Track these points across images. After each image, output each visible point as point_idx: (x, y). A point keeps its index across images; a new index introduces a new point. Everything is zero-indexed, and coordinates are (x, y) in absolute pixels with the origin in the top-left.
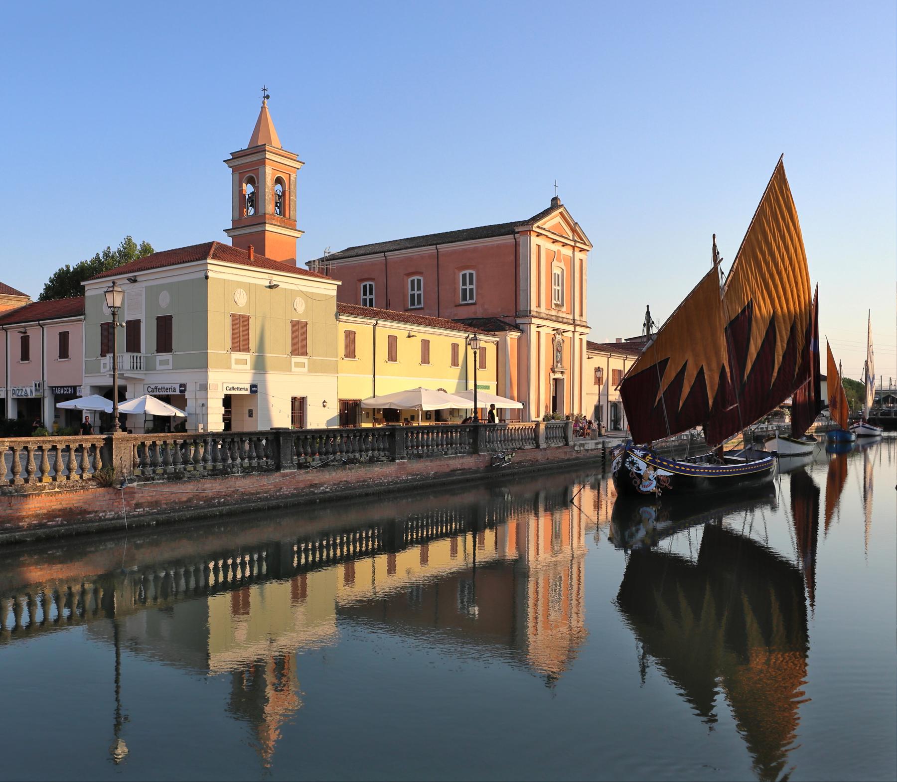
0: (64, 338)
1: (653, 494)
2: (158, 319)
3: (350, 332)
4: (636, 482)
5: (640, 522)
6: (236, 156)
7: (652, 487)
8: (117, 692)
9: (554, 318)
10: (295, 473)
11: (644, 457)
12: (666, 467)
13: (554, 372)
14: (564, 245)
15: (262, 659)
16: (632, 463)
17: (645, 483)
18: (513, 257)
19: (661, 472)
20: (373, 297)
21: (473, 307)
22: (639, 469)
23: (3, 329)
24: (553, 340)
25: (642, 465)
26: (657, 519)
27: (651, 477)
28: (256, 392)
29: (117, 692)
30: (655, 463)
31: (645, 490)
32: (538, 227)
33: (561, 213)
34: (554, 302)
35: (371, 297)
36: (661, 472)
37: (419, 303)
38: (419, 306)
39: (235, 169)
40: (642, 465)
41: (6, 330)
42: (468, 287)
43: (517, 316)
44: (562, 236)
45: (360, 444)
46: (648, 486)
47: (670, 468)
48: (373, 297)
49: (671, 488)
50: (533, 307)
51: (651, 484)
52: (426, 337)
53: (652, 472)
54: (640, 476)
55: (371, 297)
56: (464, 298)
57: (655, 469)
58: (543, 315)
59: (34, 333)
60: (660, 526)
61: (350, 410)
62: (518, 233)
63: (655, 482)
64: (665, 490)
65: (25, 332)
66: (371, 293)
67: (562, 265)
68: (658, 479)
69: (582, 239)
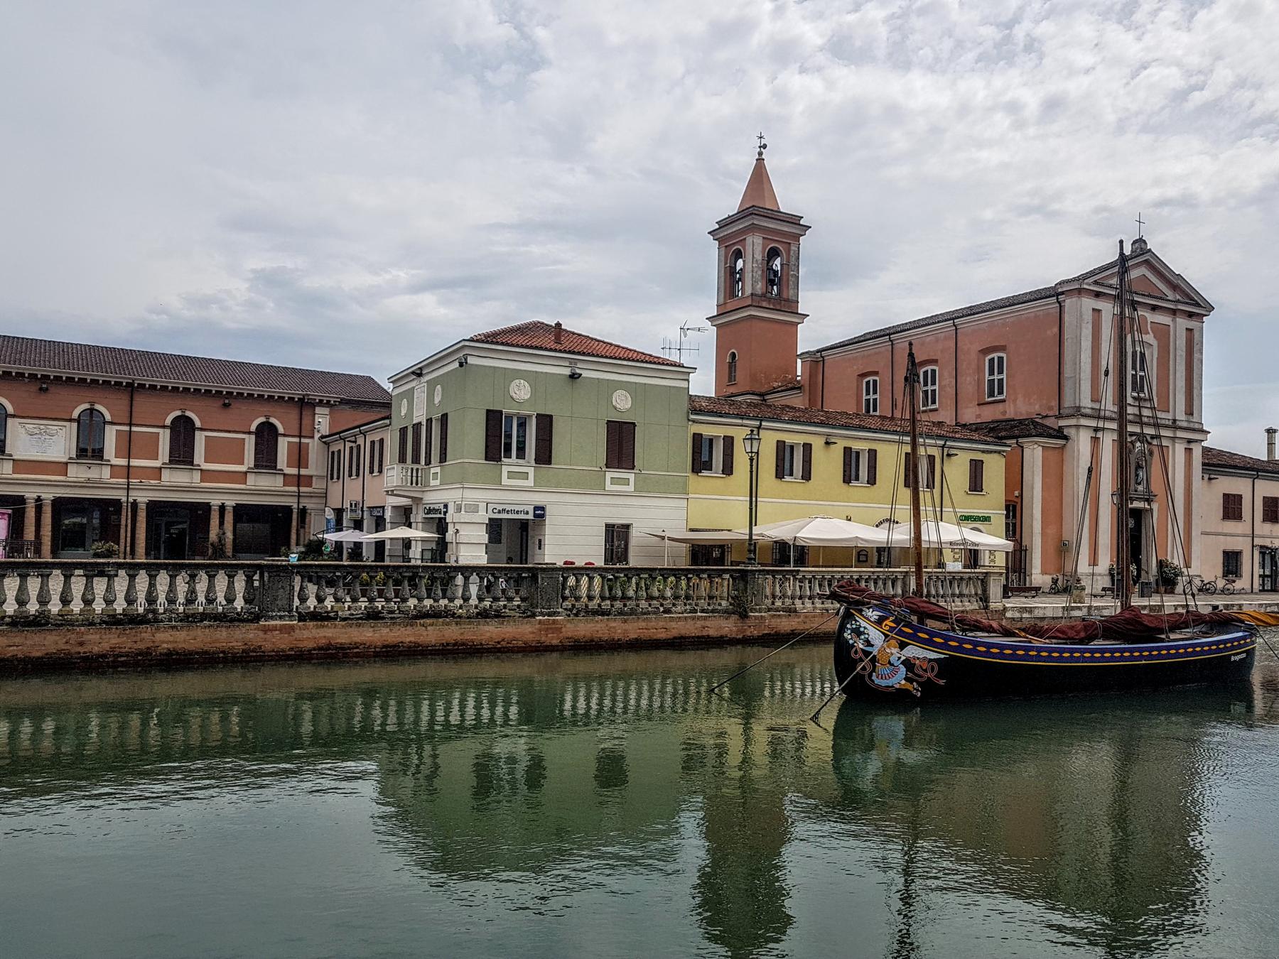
1: (902, 693)
2: (1225, 495)
5: (870, 746)
6: (723, 224)
7: (898, 680)
10: (292, 628)
11: (879, 622)
12: (929, 643)
15: (882, 842)
16: (858, 632)
17: (885, 670)
18: (1056, 330)
19: (913, 651)
20: (877, 396)
21: (1001, 405)
22: (868, 643)
25: (875, 635)
26: (908, 743)
27: (893, 659)
28: (543, 516)
30: (901, 633)
31: (883, 683)
32: (1096, 283)
36: (913, 651)
38: (933, 407)
39: (721, 241)
40: (875, 635)
42: (996, 377)
43: (1060, 417)
44: (1150, 296)
49: (942, 682)
51: (895, 672)
52: (979, 456)
53: (895, 651)
56: (991, 394)
57: (902, 646)
62: (1062, 293)
63: (903, 669)
64: (927, 686)
66: (875, 392)
68: (908, 664)
69: (1192, 299)
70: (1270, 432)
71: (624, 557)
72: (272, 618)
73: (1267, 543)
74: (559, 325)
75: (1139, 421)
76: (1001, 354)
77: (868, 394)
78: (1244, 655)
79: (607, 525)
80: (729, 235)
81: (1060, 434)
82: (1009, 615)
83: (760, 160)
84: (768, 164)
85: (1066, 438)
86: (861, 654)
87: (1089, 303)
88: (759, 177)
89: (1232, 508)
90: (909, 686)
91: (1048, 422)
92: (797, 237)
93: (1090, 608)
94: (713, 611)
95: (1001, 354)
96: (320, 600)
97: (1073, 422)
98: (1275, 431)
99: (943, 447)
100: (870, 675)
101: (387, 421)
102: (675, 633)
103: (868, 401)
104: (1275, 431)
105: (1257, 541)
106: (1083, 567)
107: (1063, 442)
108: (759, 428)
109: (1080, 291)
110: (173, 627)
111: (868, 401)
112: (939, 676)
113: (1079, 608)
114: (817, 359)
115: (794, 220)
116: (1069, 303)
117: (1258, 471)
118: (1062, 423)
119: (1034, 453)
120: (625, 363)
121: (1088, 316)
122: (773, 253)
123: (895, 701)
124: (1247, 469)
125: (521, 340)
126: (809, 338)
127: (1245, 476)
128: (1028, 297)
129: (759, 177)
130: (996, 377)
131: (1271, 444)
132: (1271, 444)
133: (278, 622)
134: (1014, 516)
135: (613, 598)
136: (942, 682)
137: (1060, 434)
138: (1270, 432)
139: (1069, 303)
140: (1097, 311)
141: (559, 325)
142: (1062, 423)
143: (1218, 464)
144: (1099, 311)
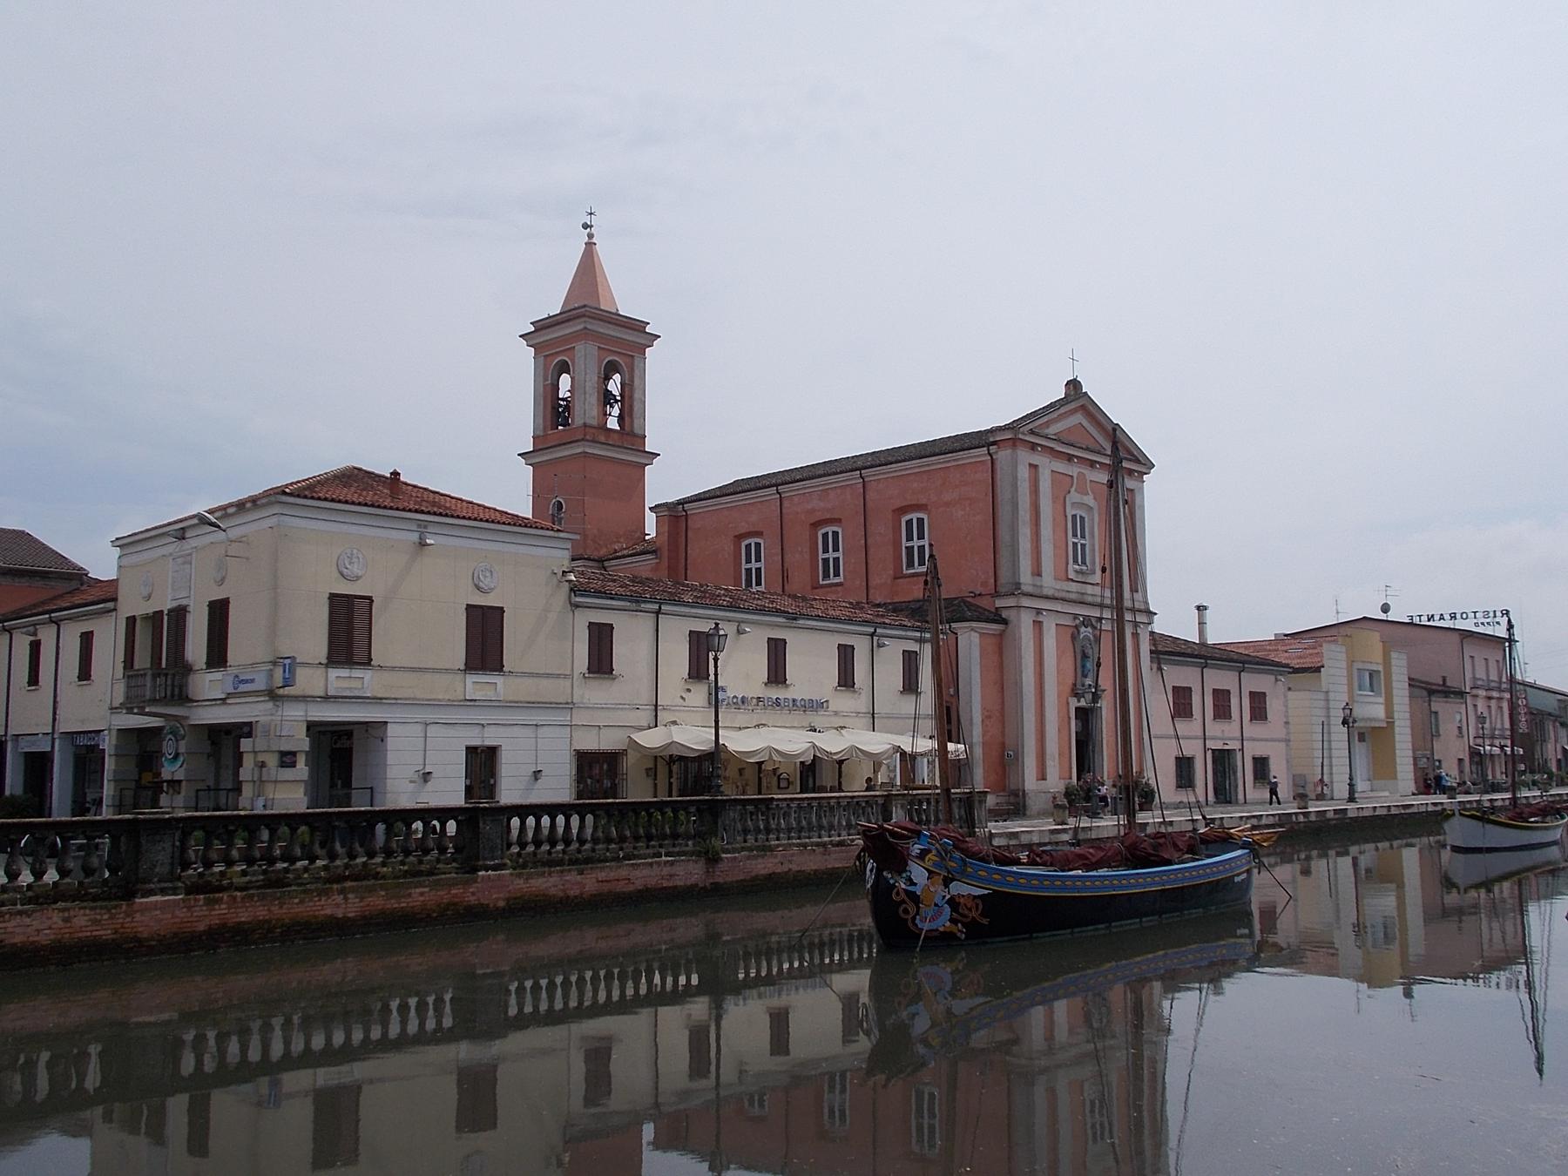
0: (87, 639)
3: (350, 598)
4: (906, 911)
6: (541, 326)
7: (943, 922)
8: (1198, 1031)
9: (1073, 596)
13: (1077, 695)
14: (1092, 464)
19: (959, 888)
23: (4, 629)
24: (1074, 638)
29: (1198, 1031)
32: (1032, 432)
33: (1083, 407)
34: (1071, 565)
35: (758, 565)
37: (837, 574)
38: (837, 580)
39: (538, 348)
41: (10, 631)
43: (996, 594)
45: (819, 818)
46: (933, 919)
47: (980, 879)
48: (761, 565)
49: (985, 921)
50: (1026, 577)
54: (914, 898)
55: (758, 565)
57: (947, 882)
58: (1046, 592)
59: (47, 636)
60: (960, 1006)
61: (596, 769)
62: (994, 443)
63: (947, 909)
65: (35, 634)
66: (758, 560)
67: (1089, 500)
68: (953, 903)
70: (1201, 609)
71: (491, 791)
72: (152, 893)
73: (1218, 745)
74: (396, 474)
75: (1133, 610)
76: (921, 515)
77: (748, 561)
78: (1244, 876)
79: (471, 750)
80: (553, 341)
81: (997, 618)
82: (996, 842)
83: (590, 245)
84: (600, 249)
85: (1005, 622)
86: (903, 895)
87: (1025, 457)
88: (589, 268)
89: (1182, 704)
90: (954, 929)
91: (984, 603)
92: (642, 349)
93: (1076, 829)
94: (679, 854)
95: (921, 515)
96: (38, 874)
97: (1010, 602)
98: (1205, 608)
99: (872, 635)
100: (914, 919)
101: (110, 605)
102: (639, 884)
103: (749, 571)
104: (1205, 608)
105: (1210, 744)
106: (1030, 782)
107: (1001, 627)
108: (658, 612)
109: (1014, 442)
110: (20, 913)
111: (749, 571)
112: (983, 915)
113: (1065, 831)
114: (675, 514)
115: (638, 326)
116: (1003, 455)
117: (1206, 658)
118: (999, 603)
119: (970, 640)
120: (365, 509)
121: (1024, 473)
122: (610, 370)
123: (941, 942)
124: (1196, 657)
125: (344, 493)
126: (664, 485)
127: (1230, 669)
128: (950, 446)
129: (589, 268)
130: (916, 543)
131: (1202, 623)
132: (1202, 623)
133: (158, 898)
134: (949, 722)
135: (609, 840)
136: (985, 921)
137: (997, 618)
138: (1201, 609)
139: (1003, 455)
140: (1034, 467)
141: (396, 474)
142: (999, 603)
143: (1169, 651)
144: (1036, 467)
